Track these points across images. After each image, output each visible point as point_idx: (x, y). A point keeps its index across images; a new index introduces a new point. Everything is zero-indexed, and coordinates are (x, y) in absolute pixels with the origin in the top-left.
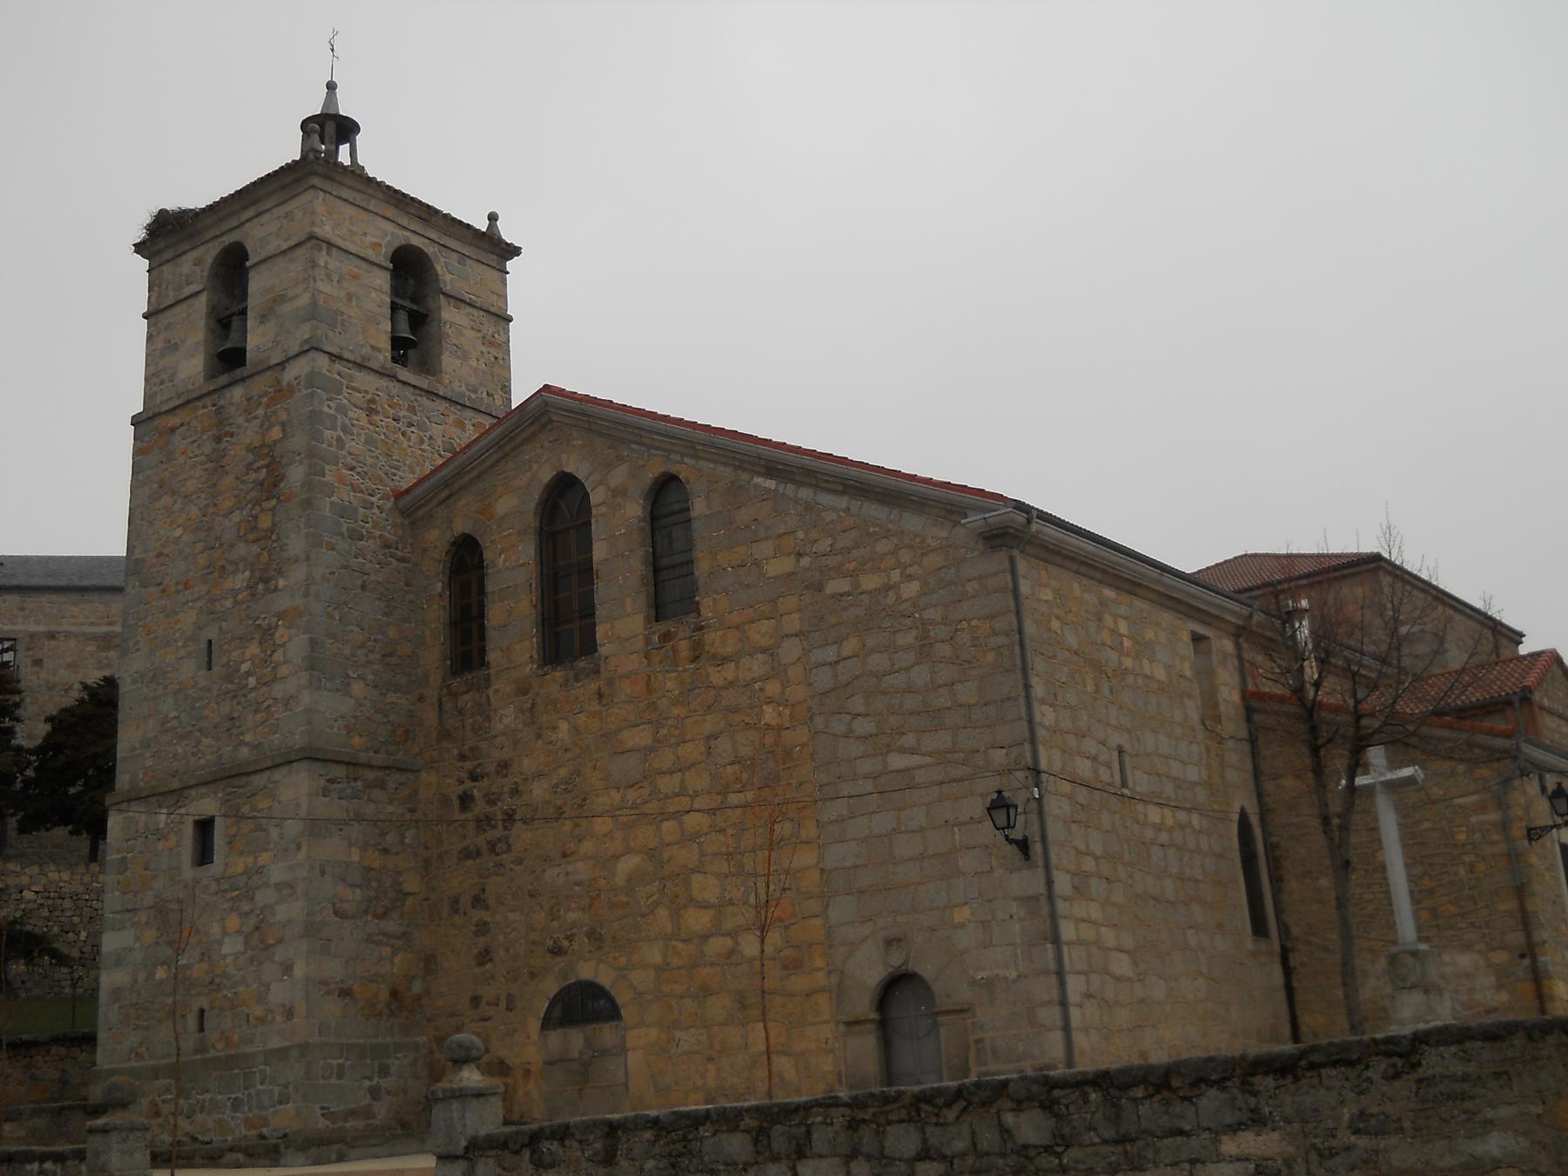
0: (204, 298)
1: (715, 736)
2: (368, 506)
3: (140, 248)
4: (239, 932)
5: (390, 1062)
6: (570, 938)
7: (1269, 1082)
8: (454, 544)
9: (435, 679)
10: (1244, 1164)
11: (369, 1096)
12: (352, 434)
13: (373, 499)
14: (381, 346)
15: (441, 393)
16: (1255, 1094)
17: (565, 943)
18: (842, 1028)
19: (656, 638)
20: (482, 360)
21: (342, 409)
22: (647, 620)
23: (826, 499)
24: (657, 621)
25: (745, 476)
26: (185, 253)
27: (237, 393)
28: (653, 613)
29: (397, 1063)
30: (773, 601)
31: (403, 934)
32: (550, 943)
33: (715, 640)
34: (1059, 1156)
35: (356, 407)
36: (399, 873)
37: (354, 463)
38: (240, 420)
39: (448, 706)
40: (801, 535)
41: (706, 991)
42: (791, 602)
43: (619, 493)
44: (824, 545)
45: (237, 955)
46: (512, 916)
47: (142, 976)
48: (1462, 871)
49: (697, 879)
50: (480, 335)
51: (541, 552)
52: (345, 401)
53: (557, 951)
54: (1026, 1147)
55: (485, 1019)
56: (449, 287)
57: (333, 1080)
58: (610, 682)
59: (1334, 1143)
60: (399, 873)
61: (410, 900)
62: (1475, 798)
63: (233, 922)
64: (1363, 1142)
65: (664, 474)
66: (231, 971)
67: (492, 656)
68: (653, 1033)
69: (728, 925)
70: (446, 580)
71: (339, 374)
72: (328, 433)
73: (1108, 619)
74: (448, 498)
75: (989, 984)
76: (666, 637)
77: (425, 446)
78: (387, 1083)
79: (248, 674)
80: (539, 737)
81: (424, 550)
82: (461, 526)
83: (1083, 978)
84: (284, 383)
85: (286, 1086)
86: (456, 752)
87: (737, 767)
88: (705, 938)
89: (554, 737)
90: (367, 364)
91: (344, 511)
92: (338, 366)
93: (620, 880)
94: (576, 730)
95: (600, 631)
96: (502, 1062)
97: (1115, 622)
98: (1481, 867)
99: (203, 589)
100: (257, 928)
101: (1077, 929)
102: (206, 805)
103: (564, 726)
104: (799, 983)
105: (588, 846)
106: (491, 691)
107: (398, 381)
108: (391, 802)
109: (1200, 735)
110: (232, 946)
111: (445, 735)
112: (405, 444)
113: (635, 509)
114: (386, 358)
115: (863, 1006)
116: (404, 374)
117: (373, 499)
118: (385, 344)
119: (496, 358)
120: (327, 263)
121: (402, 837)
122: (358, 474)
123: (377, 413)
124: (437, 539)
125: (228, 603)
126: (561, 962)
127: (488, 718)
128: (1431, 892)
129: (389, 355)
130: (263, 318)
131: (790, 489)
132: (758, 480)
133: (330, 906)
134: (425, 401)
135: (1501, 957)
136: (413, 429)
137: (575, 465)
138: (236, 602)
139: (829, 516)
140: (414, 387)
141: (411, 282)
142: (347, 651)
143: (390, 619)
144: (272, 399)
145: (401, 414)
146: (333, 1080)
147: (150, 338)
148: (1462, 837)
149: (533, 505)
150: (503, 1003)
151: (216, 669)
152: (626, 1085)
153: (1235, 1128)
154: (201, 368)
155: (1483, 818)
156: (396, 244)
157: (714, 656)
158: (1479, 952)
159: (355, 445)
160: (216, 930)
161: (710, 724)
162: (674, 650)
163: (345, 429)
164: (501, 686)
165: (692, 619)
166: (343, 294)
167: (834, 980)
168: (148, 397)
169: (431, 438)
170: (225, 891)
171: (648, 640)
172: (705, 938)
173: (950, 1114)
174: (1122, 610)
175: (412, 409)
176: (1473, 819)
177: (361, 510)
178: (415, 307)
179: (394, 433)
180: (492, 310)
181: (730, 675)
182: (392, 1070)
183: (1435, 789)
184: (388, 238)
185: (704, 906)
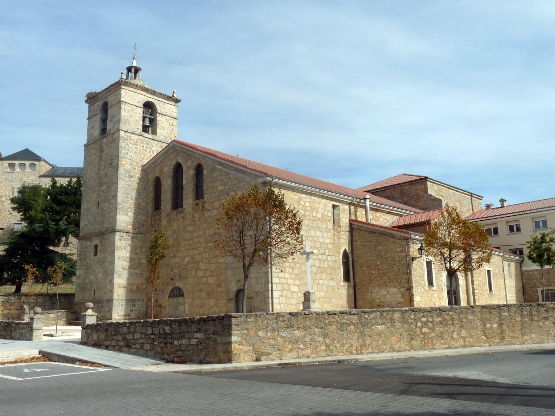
0: (99, 115)
1: (205, 229)
2: (134, 169)
3: (86, 101)
4: (102, 272)
5: (136, 303)
6: (175, 276)
7: (202, 323)
8: (155, 178)
9: (150, 211)
10: (197, 339)
11: (130, 312)
12: (130, 151)
13: (136, 167)
14: (139, 128)
15: (156, 139)
16: (200, 325)
17: (174, 277)
18: (228, 301)
19: (195, 205)
20: (169, 130)
21: (127, 145)
22: (194, 200)
23: (231, 172)
24: (196, 200)
25: (215, 165)
26: (96, 103)
27: (105, 140)
28: (195, 198)
29: (138, 304)
30: (219, 197)
31: (141, 273)
32: (171, 277)
33: (206, 205)
34: (171, 335)
35: (131, 144)
36: (140, 259)
37: (131, 158)
38: (105, 147)
39: (153, 218)
40: (225, 181)
41: (201, 291)
42: (222, 197)
43: (189, 168)
44: (230, 183)
45: (101, 277)
46: (164, 270)
47: (84, 281)
48: (396, 268)
49: (200, 264)
50: (168, 123)
51: (173, 182)
52: (129, 143)
53: (172, 279)
54: (167, 333)
55: (158, 294)
56: (160, 111)
57: (120, 307)
58: (185, 215)
59: (210, 336)
60: (140, 259)
61: (143, 265)
62: (401, 249)
63: (101, 269)
64: (214, 336)
65: (199, 163)
66: (100, 281)
67: (162, 207)
68: (190, 300)
69: (206, 275)
70: (154, 187)
71: (127, 136)
72: (123, 151)
73: (302, 203)
74: (154, 167)
75: (257, 293)
76: (197, 204)
77: (151, 153)
78: (134, 309)
79: (106, 210)
80: (171, 227)
81: (149, 180)
82: (157, 174)
83: (281, 292)
84: (114, 138)
85: (109, 308)
86: (154, 230)
87: (210, 237)
88: (202, 278)
89: (173, 228)
90: (135, 133)
91: (127, 171)
92: (127, 134)
93: (185, 263)
94: (178, 227)
95: (184, 202)
96: (160, 305)
97: (305, 203)
98: (400, 267)
99: (97, 189)
100: (105, 271)
101: (280, 280)
102: (96, 242)
103: (176, 225)
104: (220, 290)
105: (179, 255)
106: (161, 216)
107: (144, 137)
108: (138, 242)
109: (332, 231)
110: (100, 275)
111: (152, 226)
112: (145, 153)
113: (192, 172)
114: (141, 131)
115: (232, 296)
116: (145, 135)
117: (136, 167)
118: (141, 127)
119: (173, 129)
120: (125, 107)
121: (141, 250)
122: (132, 161)
123: (137, 145)
124: (152, 177)
125: (102, 193)
126: (173, 282)
127: (160, 222)
128: (389, 272)
129: (142, 130)
130: (111, 121)
131: (224, 169)
132: (218, 166)
133: (121, 267)
134: (151, 141)
135: (403, 290)
136: (148, 149)
137: (181, 161)
138: (103, 193)
139: (231, 176)
140: (148, 138)
141: (150, 110)
142: (128, 205)
143: (140, 197)
144: (112, 142)
145: (144, 145)
146: (120, 307)
147: (88, 125)
148: (396, 259)
149: (171, 170)
150: (161, 291)
151: (99, 209)
152: (184, 312)
153: (196, 332)
154: (98, 133)
155: (402, 254)
156: (145, 101)
157: (206, 209)
158: (398, 288)
159: (131, 154)
160: (97, 271)
161: (205, 226)
162: (198, 207)
163: (128, 150)
164: (164, 214)
165: (202, 200)
166: (129, 115)
167: (226, 290)
168: (88, 140)
169: (153, 151)
170: (99, 262)
171: (193, 205)
172: (202, 278)
173: (156, 326)
174: (308, 200)
175: (148, 144)
176: (400, 254)
177: (132, 170)
178: (151, 117)
179: (142, 150)
180: (172, 116)
181: (209, 214)
182: (136, 305)
183: (392, 246)
184: (143, 100)
185: (201, 270)
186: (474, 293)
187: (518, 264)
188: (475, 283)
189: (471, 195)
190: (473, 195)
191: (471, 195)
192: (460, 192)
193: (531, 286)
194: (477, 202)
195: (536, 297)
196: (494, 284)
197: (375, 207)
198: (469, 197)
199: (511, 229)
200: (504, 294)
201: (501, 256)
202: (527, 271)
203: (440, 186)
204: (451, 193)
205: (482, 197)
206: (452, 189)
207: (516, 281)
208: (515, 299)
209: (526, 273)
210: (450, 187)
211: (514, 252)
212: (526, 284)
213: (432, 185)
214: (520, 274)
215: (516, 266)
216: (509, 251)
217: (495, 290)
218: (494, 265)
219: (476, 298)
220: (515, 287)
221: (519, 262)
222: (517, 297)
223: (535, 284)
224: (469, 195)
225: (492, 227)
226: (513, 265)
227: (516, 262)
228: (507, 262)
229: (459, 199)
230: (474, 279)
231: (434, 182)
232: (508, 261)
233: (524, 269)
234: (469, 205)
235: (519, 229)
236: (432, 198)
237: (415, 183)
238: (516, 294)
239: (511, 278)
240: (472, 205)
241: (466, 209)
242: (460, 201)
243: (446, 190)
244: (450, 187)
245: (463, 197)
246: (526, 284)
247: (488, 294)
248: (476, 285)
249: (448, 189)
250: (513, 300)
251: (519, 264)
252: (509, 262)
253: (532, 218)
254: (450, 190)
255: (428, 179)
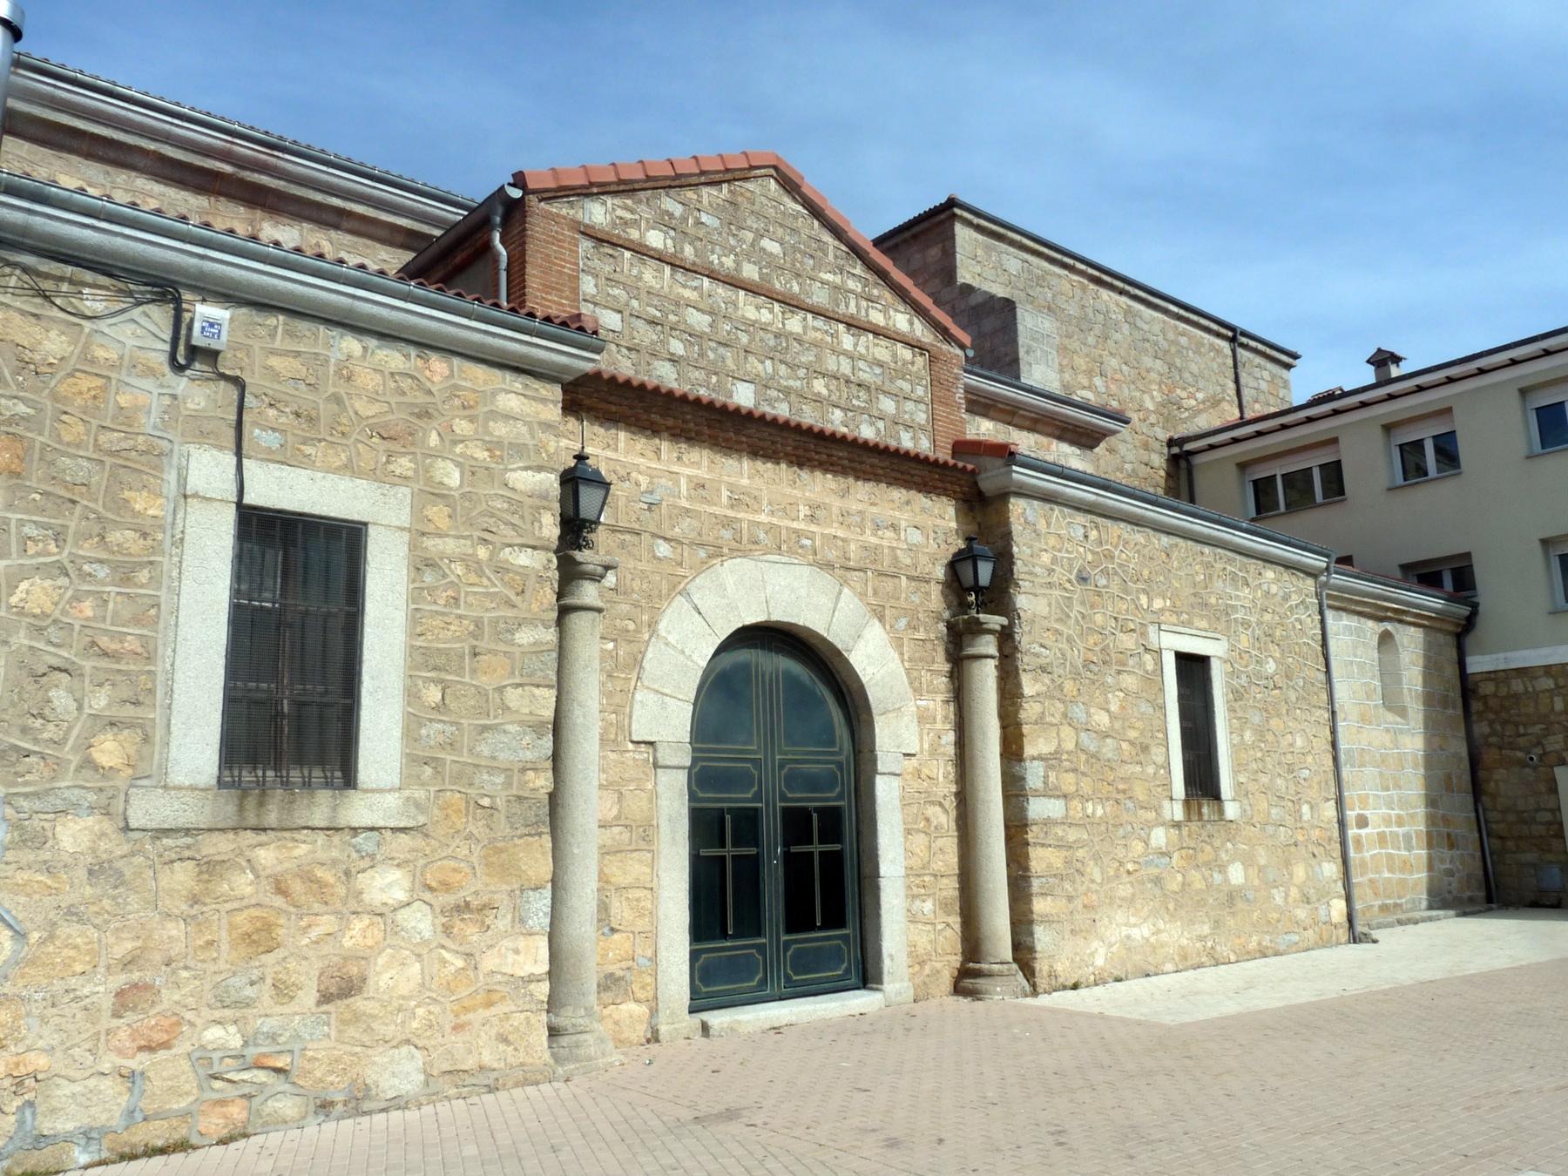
186: (1016, 829)
187: (1441, 638)
188: (1035, 745)
189: (1230, 334)
190: (1244, 340)
191: (1235, 336)
192: (1166, 312)
193: (1519, 754)
194: (1266, 375)
195: (1547, 816)
196: (1235, 749)
197: (228, 169)
198: (1225, 346)
199: (1412, 463)
200: (1330, 811)
201: (1312, 573)
202: (1492, 676)
203: (1046, 265)
204: (1113, 307)
205: (1295, 356)
206: (1121, 292)
207: (1432, 728)
208: (1422, 828)
209: (1487, 689)
210: (1105, 278)
211: (1425, 575)
212: (1489, 745)
213: (988, 248)
214: (1455, 695)
215: (1429, 647)
216: (1398, 574)
217: (1241, 791)
218: (1246, 624)
219: (1041, 859)
220: (1421, 761)
221: (1451, 628)
222: (1431, 820)
223: (1539, 743)
224: (1218, 335)
225: (1313, 461)
226: (1411, 641)
227: (1430, 624)
228: (1370, 623)
229: (1164, 344)
230: (1029, 711)
231: (997, 231)
232: (1381, 619)
233: (1478, 664)
234: (1221, 381)
235: (1448, 452)
236: (974, 300)
237: (905, 241)
238: (1431, 802)
239: (1401, 711)
240: (1237, 381)
241: (1200, 396)
242: (1166, 352)
243: (1084, 289)
244: (1105, 278)
245: (1184, 340)
246: (1489, 745)
247: (1177, 825)
248: (1049, 760)
249: (1092, 286)
250: (1407, 837)
251: (1451, 640)
252: (1389, 626)
253: (1523, 392)
254: (1105, 294)
255: (958, 211)
